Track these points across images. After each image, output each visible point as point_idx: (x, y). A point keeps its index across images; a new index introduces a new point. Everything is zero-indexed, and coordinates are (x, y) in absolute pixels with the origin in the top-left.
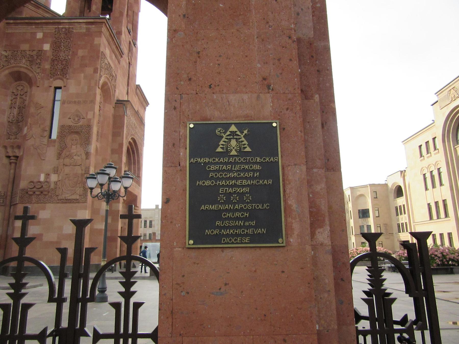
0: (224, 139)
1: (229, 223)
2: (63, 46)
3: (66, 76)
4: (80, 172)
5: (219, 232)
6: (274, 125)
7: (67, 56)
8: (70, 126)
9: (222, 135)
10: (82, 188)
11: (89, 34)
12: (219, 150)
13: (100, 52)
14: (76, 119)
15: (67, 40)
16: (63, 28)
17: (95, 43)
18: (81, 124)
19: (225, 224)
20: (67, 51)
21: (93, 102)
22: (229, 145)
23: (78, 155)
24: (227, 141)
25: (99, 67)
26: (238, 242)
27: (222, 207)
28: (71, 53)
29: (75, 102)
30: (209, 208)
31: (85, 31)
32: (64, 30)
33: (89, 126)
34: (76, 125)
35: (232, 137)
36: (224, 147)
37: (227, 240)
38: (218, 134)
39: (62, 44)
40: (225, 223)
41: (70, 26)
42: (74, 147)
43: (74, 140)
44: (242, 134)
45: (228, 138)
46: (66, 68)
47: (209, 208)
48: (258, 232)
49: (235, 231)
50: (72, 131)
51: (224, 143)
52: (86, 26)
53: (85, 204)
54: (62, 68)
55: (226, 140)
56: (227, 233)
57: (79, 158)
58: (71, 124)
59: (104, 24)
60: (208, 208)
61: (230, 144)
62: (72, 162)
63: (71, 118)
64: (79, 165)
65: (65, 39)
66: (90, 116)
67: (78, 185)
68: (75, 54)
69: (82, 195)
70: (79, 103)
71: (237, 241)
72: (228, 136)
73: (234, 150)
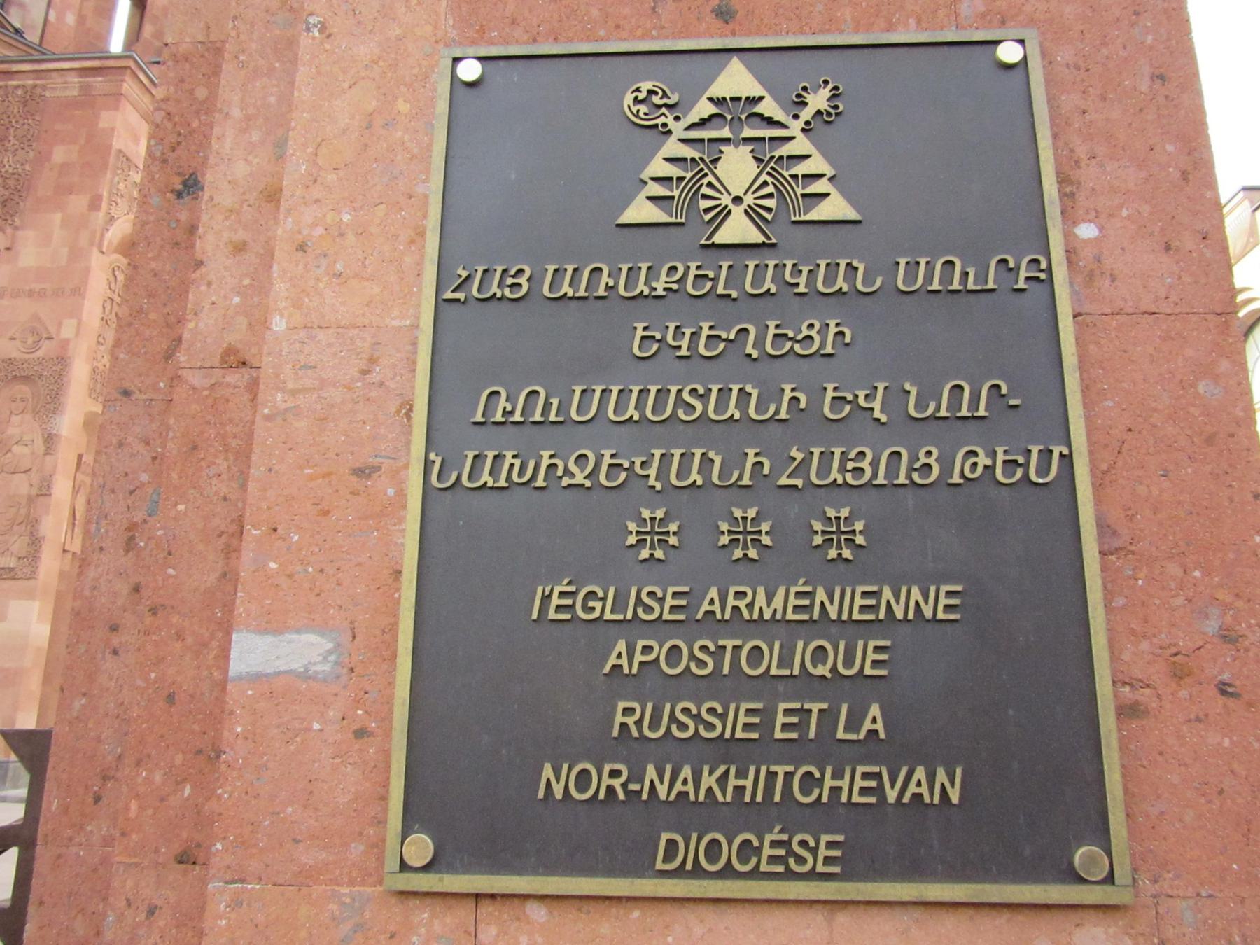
0: (673, 147)
1: (697, 718)
2: (15, 137)
3: (13, 221)
4: (24, 490)
5: (624, 785)
6: (1009, 53)
7: (22, 164)
8: (10, 361)
9: (660, 121)
10: (27, 538)
11: (87, 100)
12: (641, 211)
13: (113, 152)
14: (30, 341)
15: (24, 119)
16: (17, 87)
17: (101, 125)
18: (40, 354)
19: (674, 728)
20: (23, 149)
21: (79, 292)
22: (710, 185)
23: (25, 443)
24: (697, 155)
25: (105, 194)
26: (764, 867)
27: (912, 604)
28: (32, 154)
29: (31, 293)
30: (750, 606)
31: (76, 93)
32: (20, 92)
33: (63, 359)
34: (27, 356)
35: (726, 133)
36: (676, 193)
37: (693, 848)
38: (637, 116)
39: (12, 130)
40: (673, 718)
41: (39, 82)
42: (16, 419)
43: (18, 401)
44: (796, 117)
45: (702, 140)
46: (16, 198)
47: (750, 606)
48: (912, 789)
49: (732, 782)
50: (14, 373)
51: (673, 171)
52: (81, 80)
53: (32, 582)
54: (5, 197)
55: (688, 152)
56: (680, 793)
57: (26, 450)
58: (14, 355)
59: (129, 71)
60: (742, 604)
61: (710, 178)
62: (7, 461)
63: (14, 339)
64: (24, 472)
65: (20, 116)
66: (67, 331)
67: (16, 528)
68: (43, 158)
69: (24, 558)
70: (41, 295)
71: (754, 860)
72: (702, 123)
73: (738, 212)
